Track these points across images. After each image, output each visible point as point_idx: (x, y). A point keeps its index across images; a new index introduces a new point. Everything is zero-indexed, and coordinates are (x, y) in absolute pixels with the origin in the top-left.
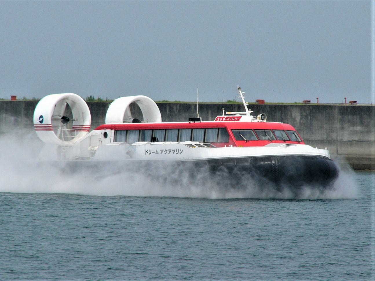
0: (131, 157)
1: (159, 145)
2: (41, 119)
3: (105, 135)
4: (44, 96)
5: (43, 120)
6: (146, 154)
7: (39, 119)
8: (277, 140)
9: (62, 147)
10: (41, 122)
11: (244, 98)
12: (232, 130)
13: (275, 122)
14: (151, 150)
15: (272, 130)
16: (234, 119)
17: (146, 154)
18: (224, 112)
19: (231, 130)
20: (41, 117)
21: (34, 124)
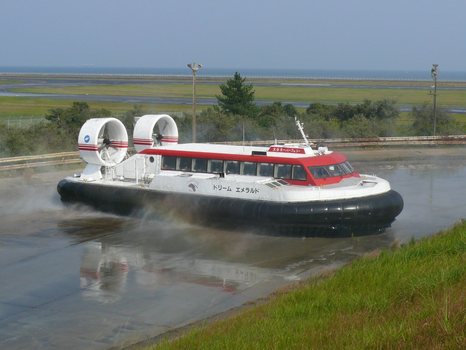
0: (194, 190)
1: (229, 178)
2: (87, 139)
3: (152, 160)
4: (89, 119)
5: (89, 139)
6: (244, 188)
7: (85, 139)
8: (333, 177)
9: (106, 167)
10: (87, 141)
11: (299, 129)
12: (309, 168)
13: (256, 155)
14: (246, 188)
15: (326, 166)
16: (294, 151)
17: (244, 188)
18: (61, 152)
19: (308, 167)
20: (87, 136)
21: (79, 143)
